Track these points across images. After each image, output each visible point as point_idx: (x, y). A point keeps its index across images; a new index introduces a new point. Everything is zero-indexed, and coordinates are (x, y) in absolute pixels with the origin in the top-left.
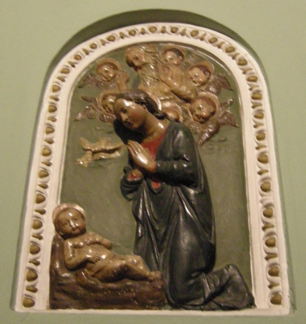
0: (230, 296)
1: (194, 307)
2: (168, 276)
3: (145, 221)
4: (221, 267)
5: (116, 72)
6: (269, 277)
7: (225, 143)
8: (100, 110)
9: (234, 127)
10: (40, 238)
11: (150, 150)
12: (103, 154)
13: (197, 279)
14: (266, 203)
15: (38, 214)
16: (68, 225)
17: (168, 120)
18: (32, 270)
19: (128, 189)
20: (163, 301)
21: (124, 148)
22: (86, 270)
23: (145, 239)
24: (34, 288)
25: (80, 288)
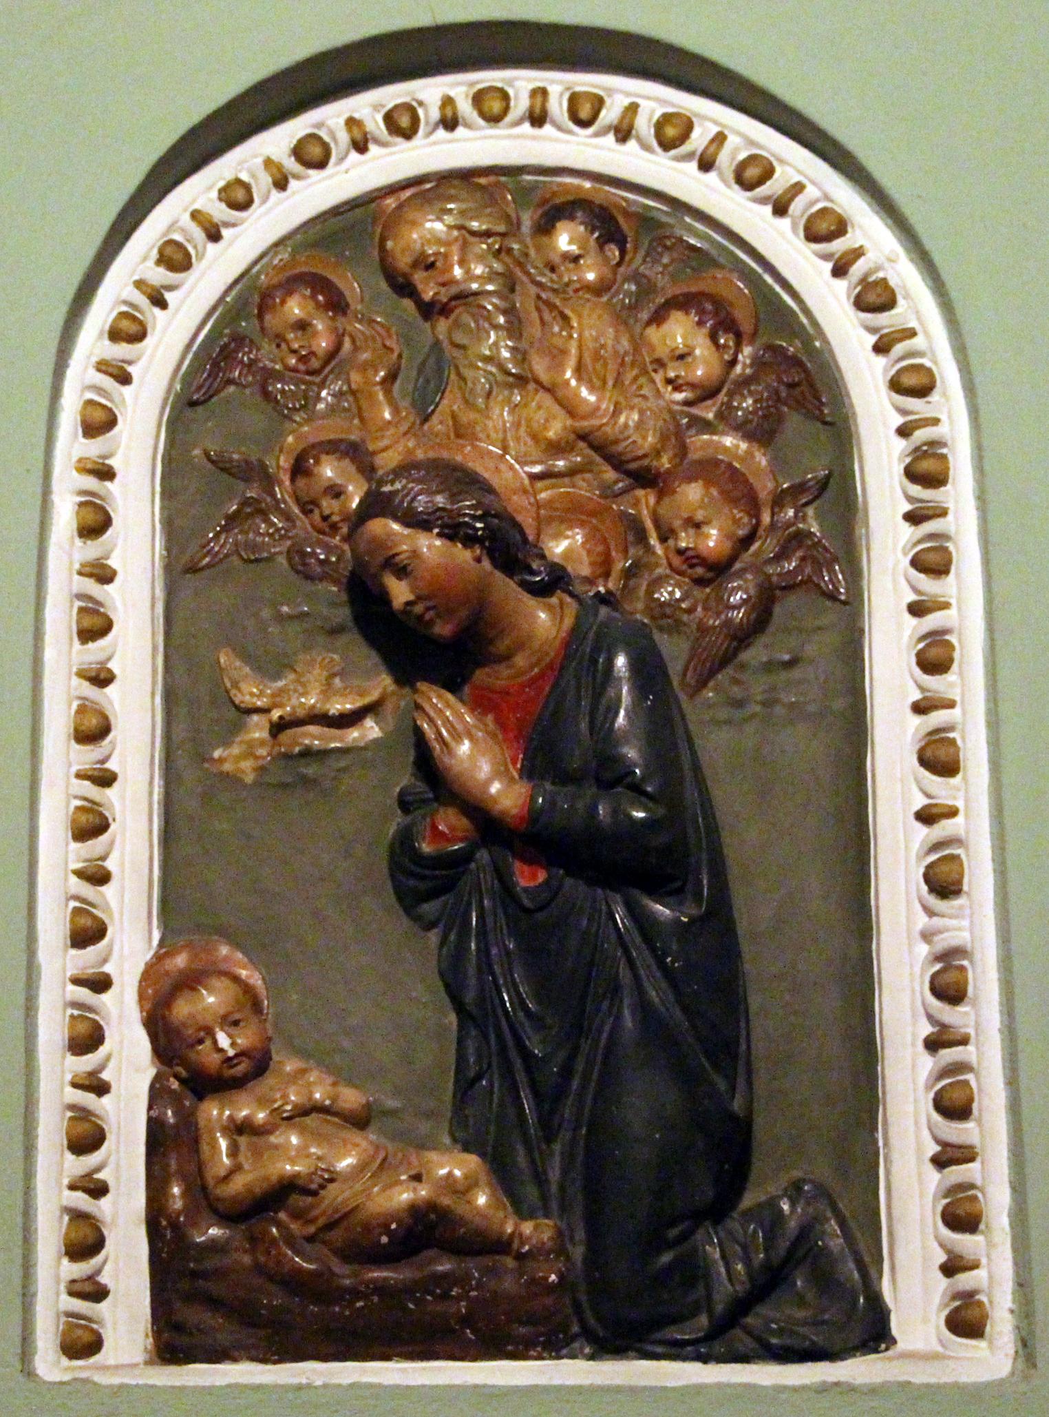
0: (801, 1302)
1: (677, 1351)
2: (580, 1234)
3: (488, 1001)
4: (773, 1189)
5: (341, 322)
6: (945, 1232)
7: (796, 673)
8: (287, 517)
9: (828, 603)
10: (101, 1089)
11: (502, 724)
12: (312, 729)
13: (686, 1246)
14: (944, 942)
15: (83, 994)
16: (208, 1043)
17: (568, 599)
18: (78, 1216)
19: (422, 886)
20: (565, 1328)
21: (400, 700)
22: (282, 1216)
23: (491, 1083)
24: (98, 1284)
25: (273, 1288)
